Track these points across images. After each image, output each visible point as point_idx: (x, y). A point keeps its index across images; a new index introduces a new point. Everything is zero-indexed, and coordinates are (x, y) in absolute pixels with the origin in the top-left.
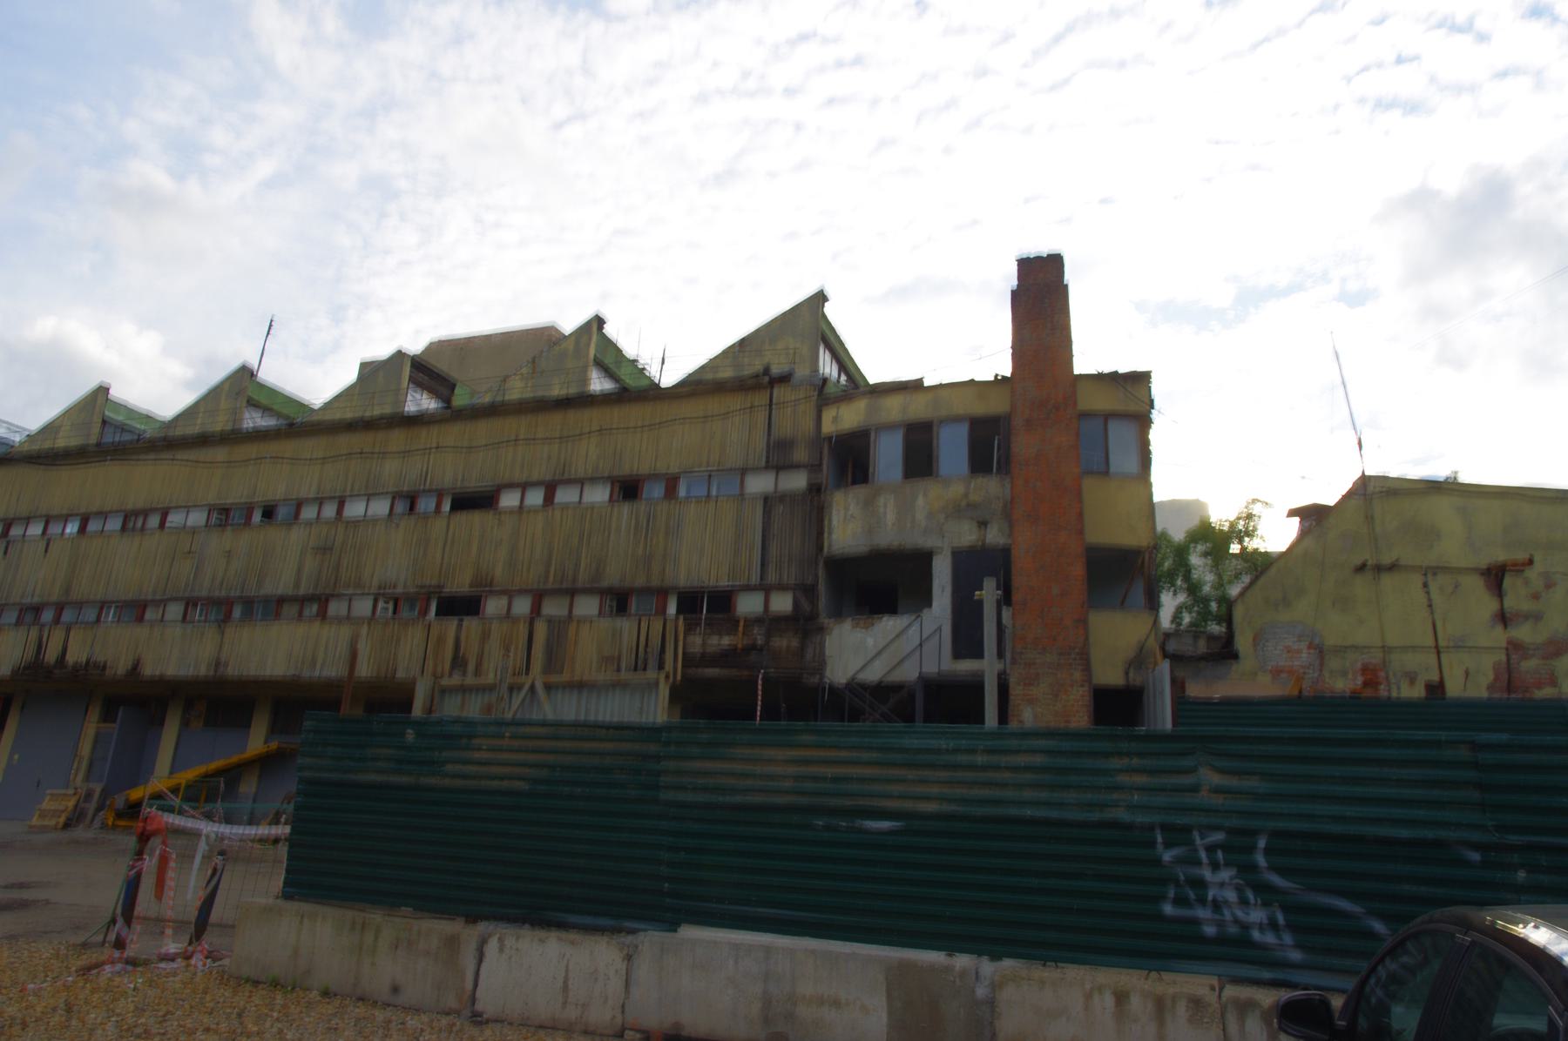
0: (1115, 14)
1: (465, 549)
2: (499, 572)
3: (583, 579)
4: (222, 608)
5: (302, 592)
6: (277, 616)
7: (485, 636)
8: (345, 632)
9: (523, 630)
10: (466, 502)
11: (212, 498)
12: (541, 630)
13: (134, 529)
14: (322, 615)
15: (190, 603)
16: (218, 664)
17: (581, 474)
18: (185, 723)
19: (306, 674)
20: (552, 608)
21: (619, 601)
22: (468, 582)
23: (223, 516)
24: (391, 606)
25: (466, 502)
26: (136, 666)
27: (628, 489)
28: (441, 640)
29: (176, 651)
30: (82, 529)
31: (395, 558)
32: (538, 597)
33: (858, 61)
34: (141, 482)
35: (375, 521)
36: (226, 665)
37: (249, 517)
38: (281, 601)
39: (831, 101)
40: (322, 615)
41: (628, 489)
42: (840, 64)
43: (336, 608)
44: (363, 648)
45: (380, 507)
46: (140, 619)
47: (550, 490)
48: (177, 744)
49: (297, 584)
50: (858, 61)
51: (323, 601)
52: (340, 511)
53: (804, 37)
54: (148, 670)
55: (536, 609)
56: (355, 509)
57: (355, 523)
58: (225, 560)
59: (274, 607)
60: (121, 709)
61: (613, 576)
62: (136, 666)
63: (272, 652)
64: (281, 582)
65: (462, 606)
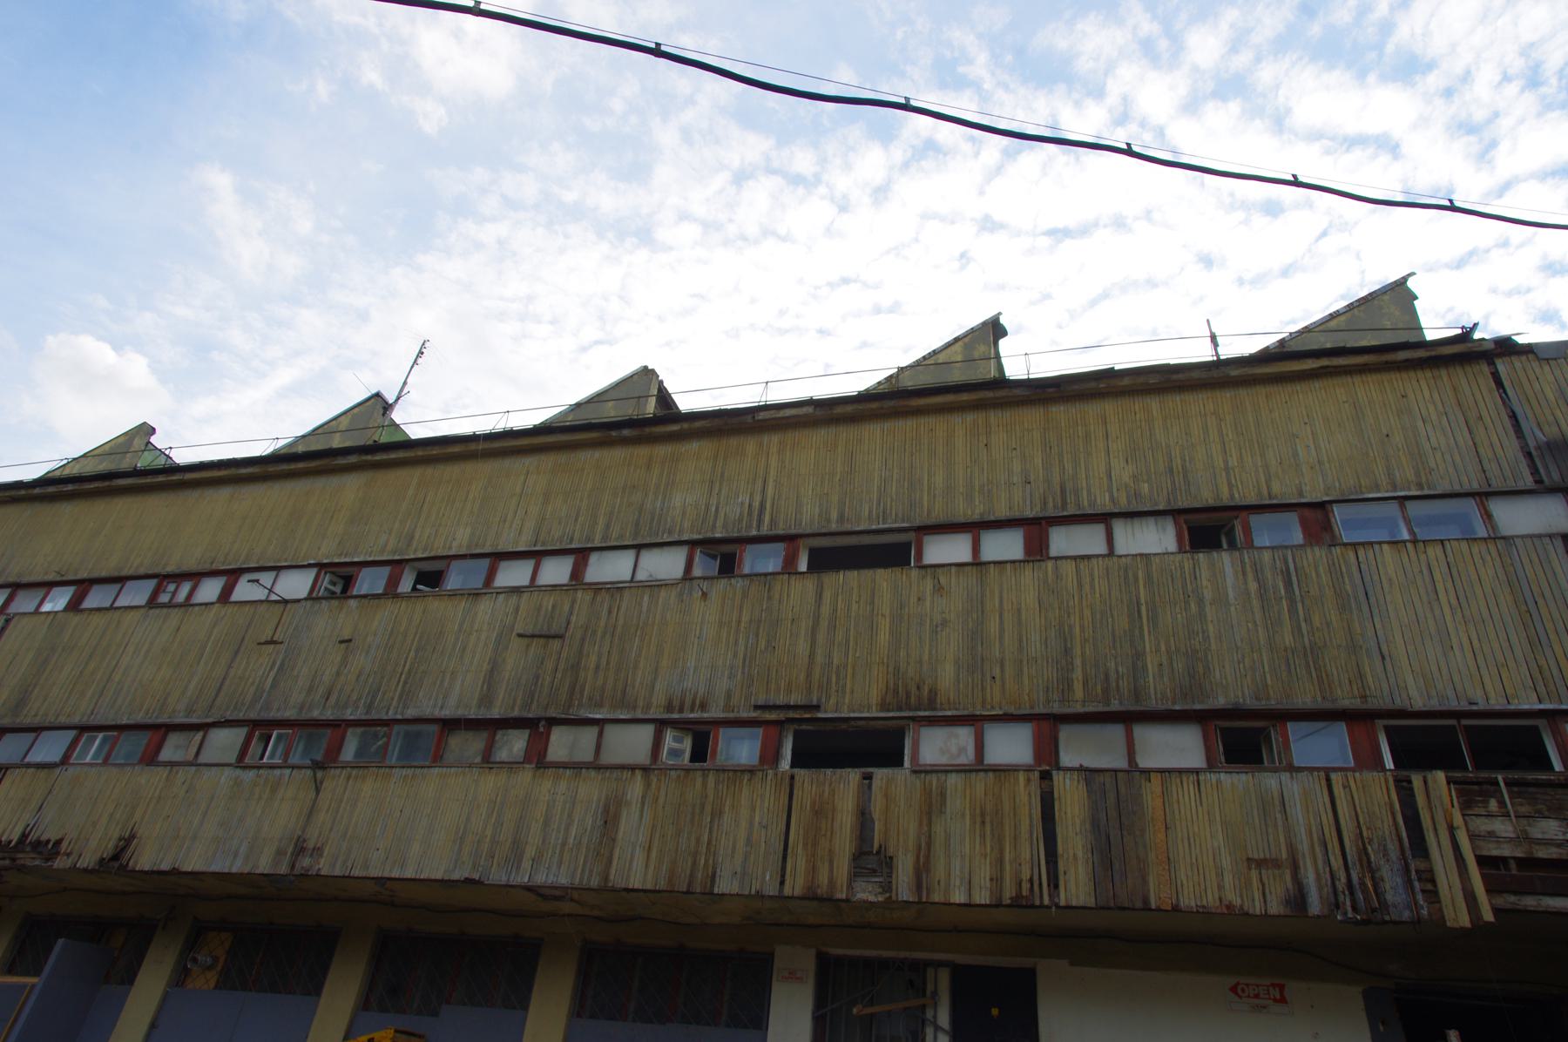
0: (1151, 284)
1: (850, 642)
2: (946, 677)
3: (1158, 692)
4: (320, 740)
5: (495, 713)
6: (437, 758)
7: (932, 806)
8: (591, 790)
9: (1026, 794)
10: (834, 555)
11: (328, 551)
12: (1072, 800)
13: (170, 605)
14: (537, 757)
15: (260, 728)
16: (300, 849)
17: (1104, 503)
18: (181, 976)
19: (498, 876)
20: (1077, 750)
21: (1243, 738)
22: (875, 696)
23: (340, 578)
24: (687, 745)
25: (834, 555)
26: (127, 842)
27: (1207, 529)
28: (821, 812)
29: (215, 823)
30: (74, 606)
31: (706, 648)
32: (1048, 726)
33: (895, 308)
34: (191, 530)
35: (655, 586)
36: (318, 851)
37: (393, 582)
38: (451, 725)
39: (864, 345)
40: (537, 757)
41: (1207, 529)
42: (877, 310)
43: (561, 744)
44: (632, 827)
45: (666, 565)
46: (150, 759)
47: (1036, 529)
48: (153, 1026)
49: (486, 699)
50: (895, 308)
51: (537, 727)
52: (577, 574)
53: (846, 281)
54: (146, 859)
55: (1047, 751)
56: (610, 568)
57: (614, 589)
58: (340, 659)
59: (431, 738)
60: (61, 941)
61: (1232, 684)
62: (127, 842)
63: (417, 829)
64: (459, 695)
65: (872, 746)
